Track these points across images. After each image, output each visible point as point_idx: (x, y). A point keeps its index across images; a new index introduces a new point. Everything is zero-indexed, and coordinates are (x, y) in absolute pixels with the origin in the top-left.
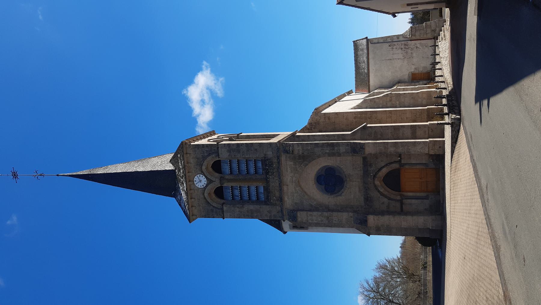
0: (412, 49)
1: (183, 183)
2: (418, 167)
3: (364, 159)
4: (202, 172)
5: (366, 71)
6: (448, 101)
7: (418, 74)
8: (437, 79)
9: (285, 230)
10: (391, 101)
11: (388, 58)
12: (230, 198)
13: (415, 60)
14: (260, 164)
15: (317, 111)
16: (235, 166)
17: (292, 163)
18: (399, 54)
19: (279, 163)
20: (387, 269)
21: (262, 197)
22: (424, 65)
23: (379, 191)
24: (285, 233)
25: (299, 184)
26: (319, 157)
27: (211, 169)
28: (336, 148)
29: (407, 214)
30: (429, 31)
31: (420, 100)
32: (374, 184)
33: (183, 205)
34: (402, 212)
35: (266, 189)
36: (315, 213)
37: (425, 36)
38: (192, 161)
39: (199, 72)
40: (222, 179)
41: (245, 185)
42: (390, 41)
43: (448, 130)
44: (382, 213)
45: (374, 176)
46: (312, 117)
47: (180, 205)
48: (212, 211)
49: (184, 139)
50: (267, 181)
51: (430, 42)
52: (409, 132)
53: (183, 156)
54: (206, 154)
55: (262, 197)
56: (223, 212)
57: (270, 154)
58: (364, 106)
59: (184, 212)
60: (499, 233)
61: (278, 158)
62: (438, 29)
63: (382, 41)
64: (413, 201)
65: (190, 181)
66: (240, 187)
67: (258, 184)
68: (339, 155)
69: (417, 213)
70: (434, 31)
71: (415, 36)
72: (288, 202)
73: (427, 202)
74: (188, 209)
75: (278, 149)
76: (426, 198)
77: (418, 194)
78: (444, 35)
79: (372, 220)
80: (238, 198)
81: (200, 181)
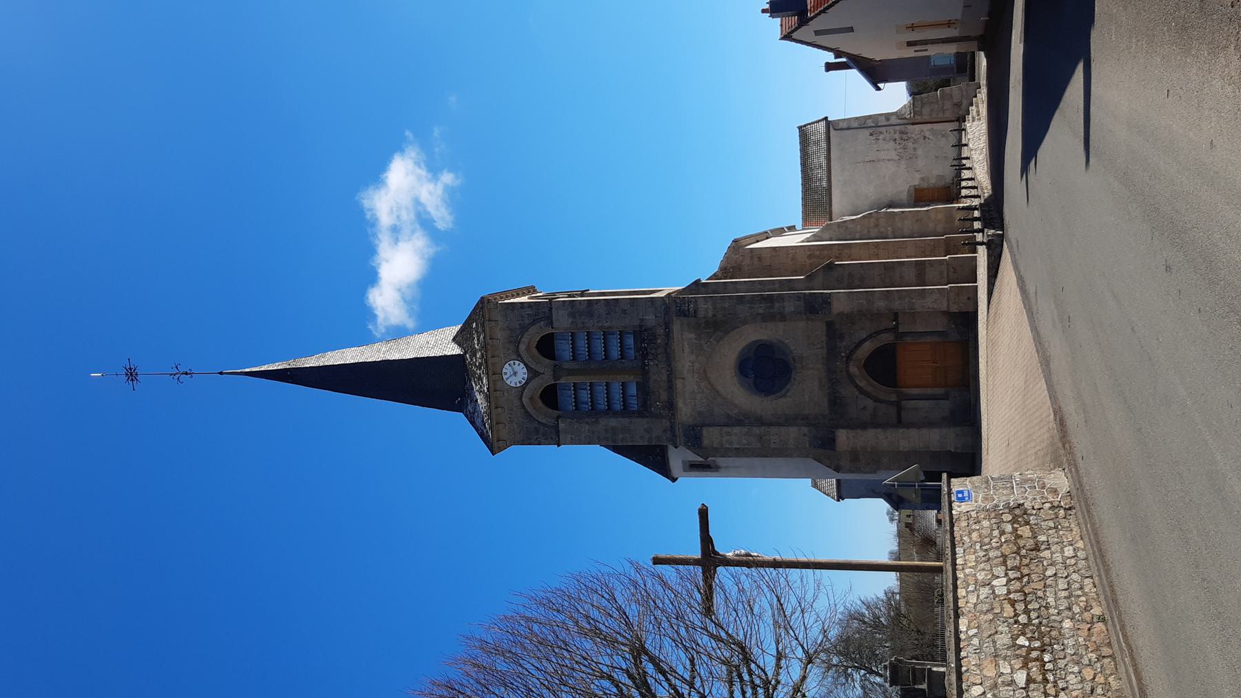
0: (915, 142)
1: (480, 379)
2: (929, 339)
3: (830, 325)
4: (519, 355)
5: (824, 184)
6: (982, 212)
7: (928, 189)
8: (964, 192)
9: (675, 475)
10: (877, 226)
11: (867, 159)
12: (572, 407)
13: (921, 163)
14: (630, 341)
15: (737, 245)
16: (582, 343)
17: (692, 336)
18: (888, 150)
19: (668, 335)
20: (865, 623)
21: (634, 404)
22: (940, 171)
23: (857, 386)
24: (674, 480)
25: (706, 376)
26: (744, 322)
27: (535, 351)
28: (777, 305)
29: (909, 426)
30: (948, 105)
31: (931, 225)
32: (848, 372)
33: (478, 422)
34: (900, 423)
35: (643, 388)
36: (736, 430)
37: (941, 115)
38: (499, 334)
39: (363, 294)
40: (557, 371)
41: (600, 381)
42: (871, 125)
43: (982, 255)
44: (864, 426)
45: (849, 358)
46: (727, 257)
47: (472, 423)
48: (537, 431)
49: (485, 294)
50: (645, 372)
51: (955, 125)
52: (911, 274)
53: (483, 326)
54: (527, 322)
55: (634, 404)
56: (558, 432)
57: (650, 319)
58: (827, 235)
59: (482, 435)
60: (1070, 409)
61: (667, 326)
62: (965, 102)
63: (856, 125)
64: (922, 404)
65: (495, 374)
66: (591, 385)
67: (626, 378)
68: (783, 318)
69: (929, 424)
70: (958, 105)
71: (921, 114)
72: (685, 412)
73: (946, 405)
74: (491, 428)
75: (667, 309)
76: (945, 397)
77: (929, 391)
78: (978, 112)
79: (844, 438)
80: (588, 407)
81: (515, 373)
